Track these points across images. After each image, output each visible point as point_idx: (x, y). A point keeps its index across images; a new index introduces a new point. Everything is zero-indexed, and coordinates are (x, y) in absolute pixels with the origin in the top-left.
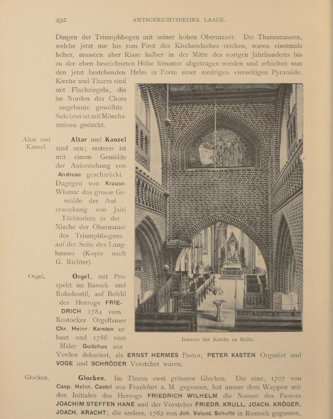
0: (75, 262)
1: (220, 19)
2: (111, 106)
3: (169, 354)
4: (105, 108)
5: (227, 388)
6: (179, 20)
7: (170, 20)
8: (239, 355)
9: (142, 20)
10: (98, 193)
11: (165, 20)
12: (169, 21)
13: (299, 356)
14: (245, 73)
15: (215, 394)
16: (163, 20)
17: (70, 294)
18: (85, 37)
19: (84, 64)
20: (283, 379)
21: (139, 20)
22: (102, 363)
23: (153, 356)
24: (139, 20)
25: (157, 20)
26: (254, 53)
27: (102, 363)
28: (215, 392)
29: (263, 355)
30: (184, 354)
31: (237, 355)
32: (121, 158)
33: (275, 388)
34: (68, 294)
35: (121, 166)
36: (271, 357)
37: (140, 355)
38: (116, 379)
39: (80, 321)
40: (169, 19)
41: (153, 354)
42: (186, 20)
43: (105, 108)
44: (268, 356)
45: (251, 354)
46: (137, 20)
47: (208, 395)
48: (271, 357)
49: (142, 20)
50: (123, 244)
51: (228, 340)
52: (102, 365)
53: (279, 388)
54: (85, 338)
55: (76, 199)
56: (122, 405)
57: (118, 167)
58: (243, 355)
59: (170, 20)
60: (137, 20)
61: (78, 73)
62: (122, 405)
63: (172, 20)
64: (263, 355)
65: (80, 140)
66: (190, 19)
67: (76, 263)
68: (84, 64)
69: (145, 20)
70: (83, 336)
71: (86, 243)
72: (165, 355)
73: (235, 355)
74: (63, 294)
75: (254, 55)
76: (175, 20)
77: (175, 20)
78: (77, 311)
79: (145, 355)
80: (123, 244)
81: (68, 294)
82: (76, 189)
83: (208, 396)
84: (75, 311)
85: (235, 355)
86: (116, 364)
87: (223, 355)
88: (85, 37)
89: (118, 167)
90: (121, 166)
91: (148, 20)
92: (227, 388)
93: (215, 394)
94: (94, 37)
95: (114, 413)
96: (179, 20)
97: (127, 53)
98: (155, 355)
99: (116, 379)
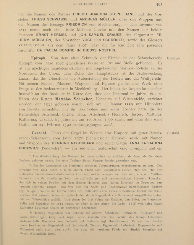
3: (61, 99)
8: (60, 19)
13: (98, 84)
19: (147, 63)
20: (79, 138)
22: (101, 13)
23: (53, 144)
26: (138, 93)
27: (101, 13)
29: (73, 133)
31: (128, 14)
36: (141, 36)
37: (44, 35)
39: (151, 58)
41: (52, 34)
44: (76, 133)
45: (48, 40)
48: (141, 36)
50: (120, 24)
52: (109, 40)
54: (154, 149)
56: (151, 143)
57: (91, 25)
58: (112, 14)
62: (151, 143)
64: (73, 133)
72: (59, 35)
73: (144, 143)
75: (138, 94)
79: (47, 35)
80: (120, 24)
85: (144, 143)
86: (117, 40)
87: (56, 34)
89: (91, 25)
97: (151, 132)
98: (54, 143)
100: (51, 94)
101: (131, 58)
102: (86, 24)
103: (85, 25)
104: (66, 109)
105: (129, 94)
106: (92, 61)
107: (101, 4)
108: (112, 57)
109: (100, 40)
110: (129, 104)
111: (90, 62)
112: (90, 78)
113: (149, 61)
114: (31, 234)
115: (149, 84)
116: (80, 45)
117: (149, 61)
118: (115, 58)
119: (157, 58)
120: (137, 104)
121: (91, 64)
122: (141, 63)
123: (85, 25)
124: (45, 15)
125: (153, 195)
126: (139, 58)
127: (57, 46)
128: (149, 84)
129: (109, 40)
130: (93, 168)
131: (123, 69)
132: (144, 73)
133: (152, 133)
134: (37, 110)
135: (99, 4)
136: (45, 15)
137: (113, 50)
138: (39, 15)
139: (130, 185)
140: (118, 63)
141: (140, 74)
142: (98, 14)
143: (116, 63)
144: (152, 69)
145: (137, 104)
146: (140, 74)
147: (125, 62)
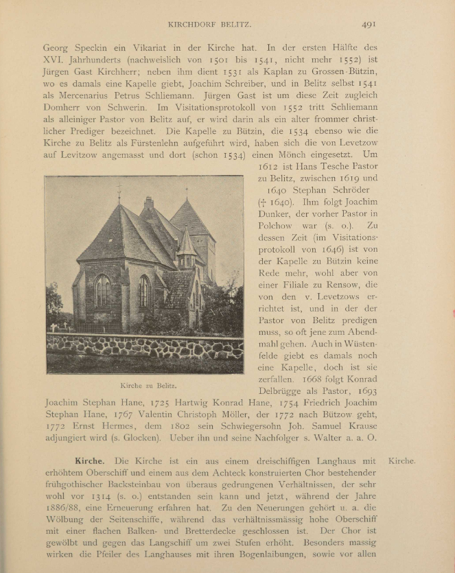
0: (51, 132)
2: (67, 541)
4: (59, 544)
5: (85, 544)
14: (106, 474)
17: (248, 108)
18: (191, 48)
19: (159, 73)
20: (129, 415)
30: (345, 212)
34: (245, 108)
39: (63, 555)
43: (59, 544)
51: (140, 387)
55: (269, 353)
61: (277, 497)
65: (194, 108)
67: (155, 97)
68: (159, 73)
74: (238, 108)
81: (245, 108)
82: (285, 209)
88: (191, 48)
92: (85, 544)
94: (81, 403)
95: (82, 555)
97: (262, 271)
104: (53, 529)
105: (280, 167)
106: (232, 409)
107: (235, 24)
108: (107, 70)
110: (292, 107)
113: (161, 549)
116: (175, 426)
117: (161, 549)
118: (113, 73)
119: (205, 85)
120: (314, 60)
125: (338, 143)
131: (256, 403)
132: (279, 437)
133: (264, 274)
134: (322, 84)
135: (231, 24)
140: (253, 497)
141: (318, 345)
143: (248, 497)
145: (314, 60)
146: (318, 345)
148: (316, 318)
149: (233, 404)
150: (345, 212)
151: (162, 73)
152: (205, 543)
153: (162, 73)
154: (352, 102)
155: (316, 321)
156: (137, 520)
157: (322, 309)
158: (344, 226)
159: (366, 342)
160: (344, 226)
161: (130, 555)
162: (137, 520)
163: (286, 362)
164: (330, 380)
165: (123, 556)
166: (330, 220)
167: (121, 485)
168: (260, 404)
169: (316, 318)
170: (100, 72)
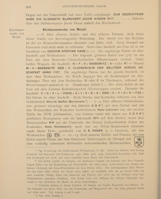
1: (104, 6)
6: (84, 6)
7: (80, 6)
9: (67, 6)
10: (53, 119)
11: (78, 6)
12: (80, 7)
15: (27, 68)
16: (77, 6)
21: (65, 6)
24: (65, 6)
25: (74, 6)
28: (53, 66)
30: (122, 50)
32: (32, 102)
33: (111, 60)
35: (51, 39)
38: (58, 98)
40: (80, 6)
42: (88, 6)
46: (64, 6)
47: (110, 67)
49: (67, 6)
52: (55, 52)
53: (113, 60)
57: (50, 39)
59: (80, 6)
60: (64, 6)
63: (81, 6)
66: (89, 6)
68: (89, 144)
69: (68, 6)
70: (67, 117)
71: (87, 113)
76: (83, 6)
77: (83, 6)
78: (131, 67)
83: (111, 68)
84: (130, 68)
89: (50, 39)
90: (51, 39)
91: (70, 6)
93: (27, 68)
96: (84, 6)
97: (28, 126)
98: (126, 63)
99: (58, 98)
100: (53, 60)
101: (116, 150)
102: (40, 19)
103: (40, 20)
109: (130, 139)
111: (49, 55)
112: (66, 109)
114: (95, 189)
115: (53, 56)
121: (50, 56)
122: (31, 119)
123: (40, 20)
124: (34, 15)
126: (107, 179)
127: (65, 140)
128: (53, 56)
129: (55, 52)
130: (91, 176)
136: (34, 15)
137: (140, 14)
138: (103, 60)
139: (53, 58)
142: (53, 51)
144: (141, 55)
147: (42, 23)
148: (81, 38)
149: (47, 43)
150: (122, 50)
151: (122, 97)
152: (48, 158)
153: (122, 97)
154: (83, 58)
155: (81, 39)
156: (62, 64)
157: (46, 47)
158: (92, 51)
159: (39, 84)
160: (92, 51)
161: (35, 23)
162: (62, 64)
163: (36, 108)
164: (82, 56)
165: (33, 24)
166: (107, 129)
167: (42, 39)
168: (60, 144)
169: (81, 38)
170: (44, 43)
